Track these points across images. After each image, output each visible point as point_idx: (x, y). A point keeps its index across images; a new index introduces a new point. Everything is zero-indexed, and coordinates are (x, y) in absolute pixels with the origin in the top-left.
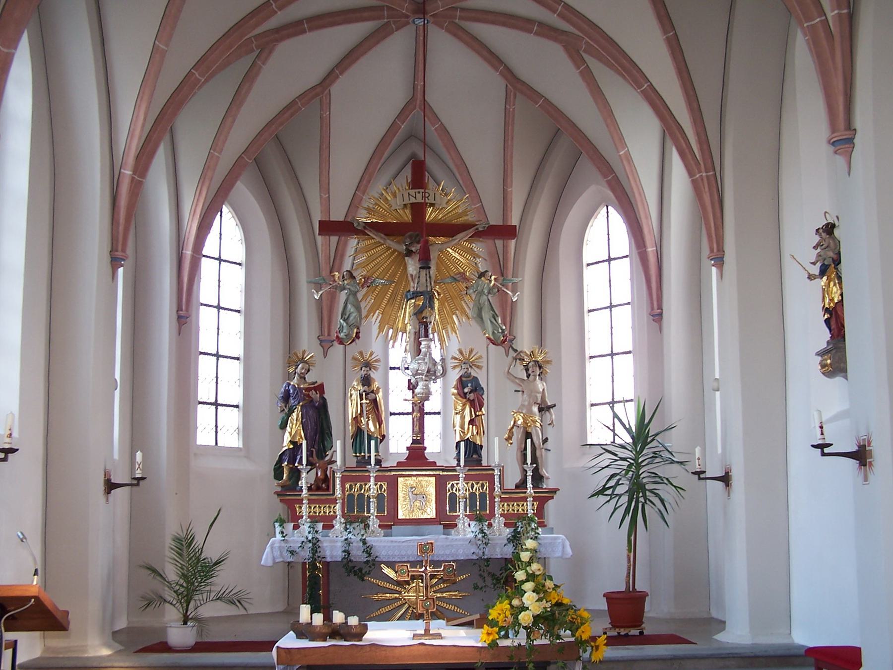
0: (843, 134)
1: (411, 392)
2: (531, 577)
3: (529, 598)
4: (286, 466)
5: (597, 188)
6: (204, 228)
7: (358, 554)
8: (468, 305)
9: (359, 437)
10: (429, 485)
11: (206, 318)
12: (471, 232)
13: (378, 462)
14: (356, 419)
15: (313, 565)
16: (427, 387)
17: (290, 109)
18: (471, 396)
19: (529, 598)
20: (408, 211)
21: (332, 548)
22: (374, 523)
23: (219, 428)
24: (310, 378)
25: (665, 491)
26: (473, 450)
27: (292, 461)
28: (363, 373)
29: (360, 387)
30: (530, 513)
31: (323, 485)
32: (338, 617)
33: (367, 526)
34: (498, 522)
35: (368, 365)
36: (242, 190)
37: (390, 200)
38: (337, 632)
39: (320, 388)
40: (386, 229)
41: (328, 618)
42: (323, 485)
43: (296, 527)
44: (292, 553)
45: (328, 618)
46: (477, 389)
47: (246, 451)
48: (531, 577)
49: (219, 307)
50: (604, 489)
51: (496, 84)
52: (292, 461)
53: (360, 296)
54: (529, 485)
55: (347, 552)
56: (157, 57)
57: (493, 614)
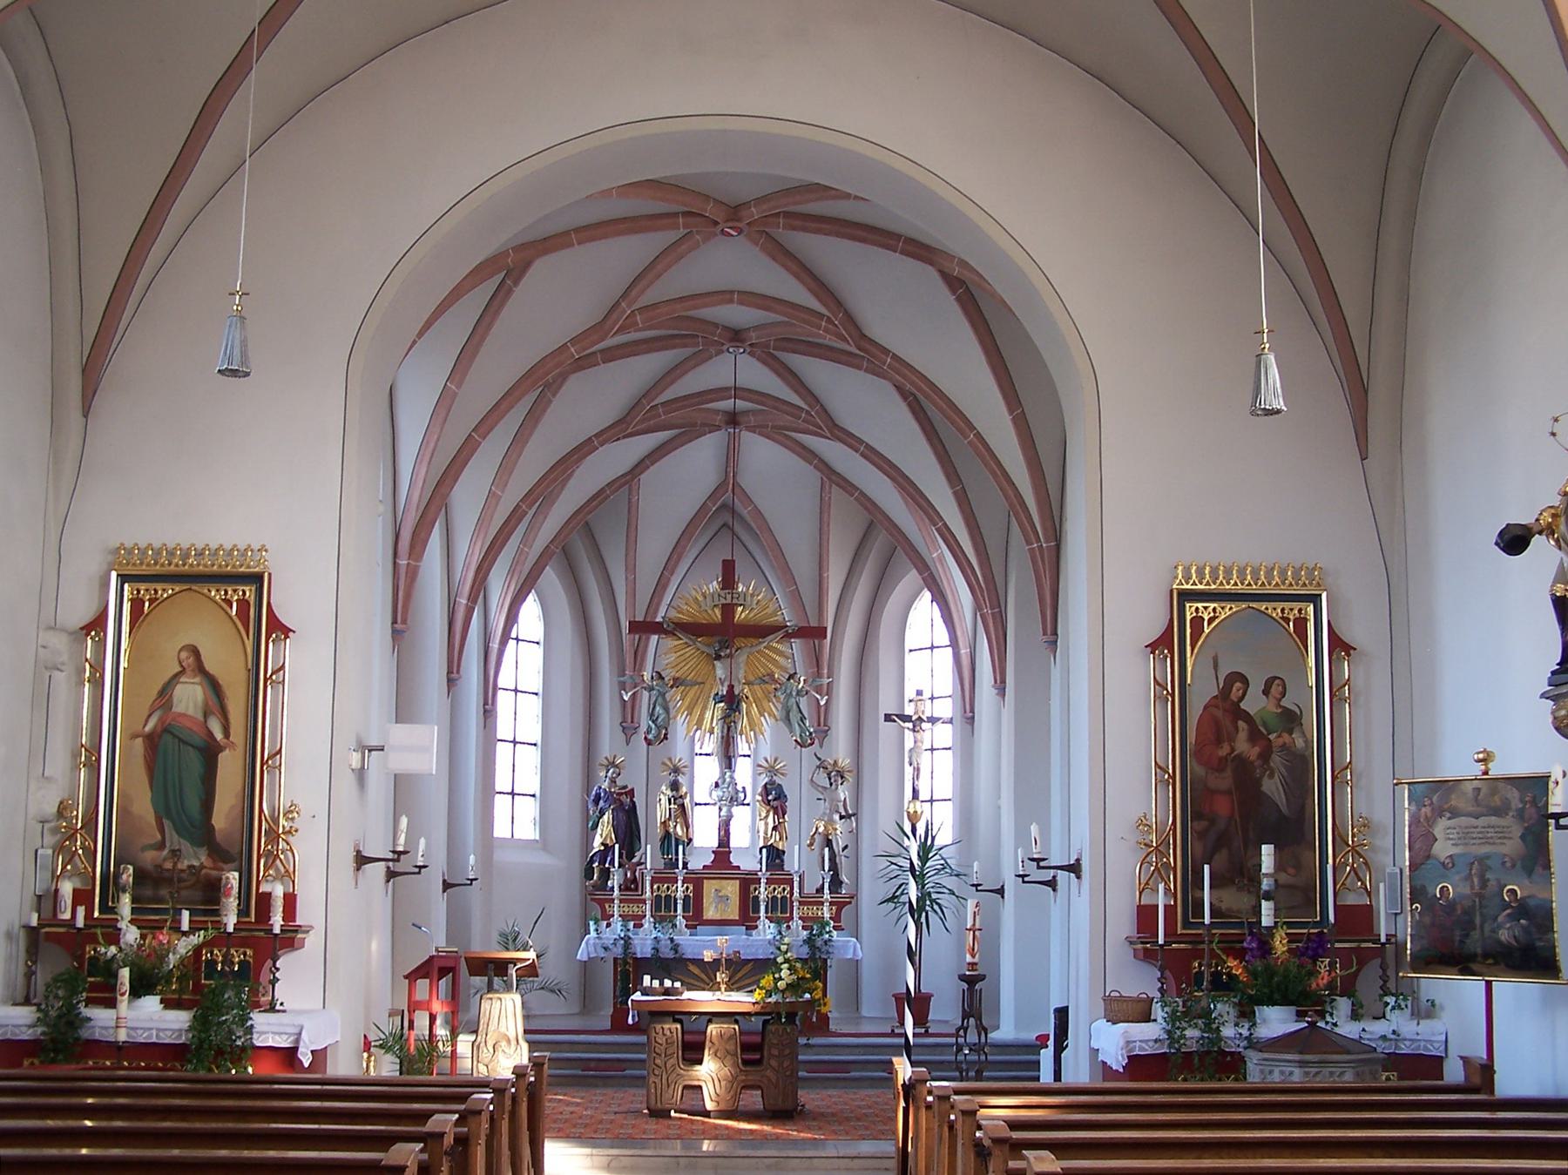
0: (1052, 638)
1: (718, 800)
2: (787, 961)
3: (785, 973)
4: (594, 869)
5: (912, 577)
6: (512, 618)
7: (666, 952)
8: (775, 708)
9: (668, 842)
10: (732, 889)
11: (504, 701)
12: (780, 634)
13: (685, 865)
14: (664, 823)
15: (624, 960)
16: (729, 811)
17: (599, 497)
18: (775, 803)
19: (785, 973)
20: (718, 612)
21: (643, 945)
22: (680, 921)
23: (517, 820)
24: (620, 782)
25: (945, 900)
26: (775, 856)
27: (602, 862)
28: (672, 778)
29: (669, 792)
30: (827, 916)
31: (631, 886)
32: (668, 983)
33: (674, 926)
34: (797, 924)
35: (676, 770)
36: (550, 577)
37: (697, 592)
38: (667, 992)
39: (631, 793)
40: (693, 630)
41: (662, 984)
42: (631, 886)
43: (608, 925)
44: (606, 949)
45: (662, 984)
46: (781, 796)
47: (544, 843)
48: (787, 961)
49: (516, 691)
50: (894, 897)
51: (812, 476)
52: (602, 862)
53: (668, 696)
54: (826, 890)
55: (656, 949)
56: (446, 400)
57: (763, 983)
